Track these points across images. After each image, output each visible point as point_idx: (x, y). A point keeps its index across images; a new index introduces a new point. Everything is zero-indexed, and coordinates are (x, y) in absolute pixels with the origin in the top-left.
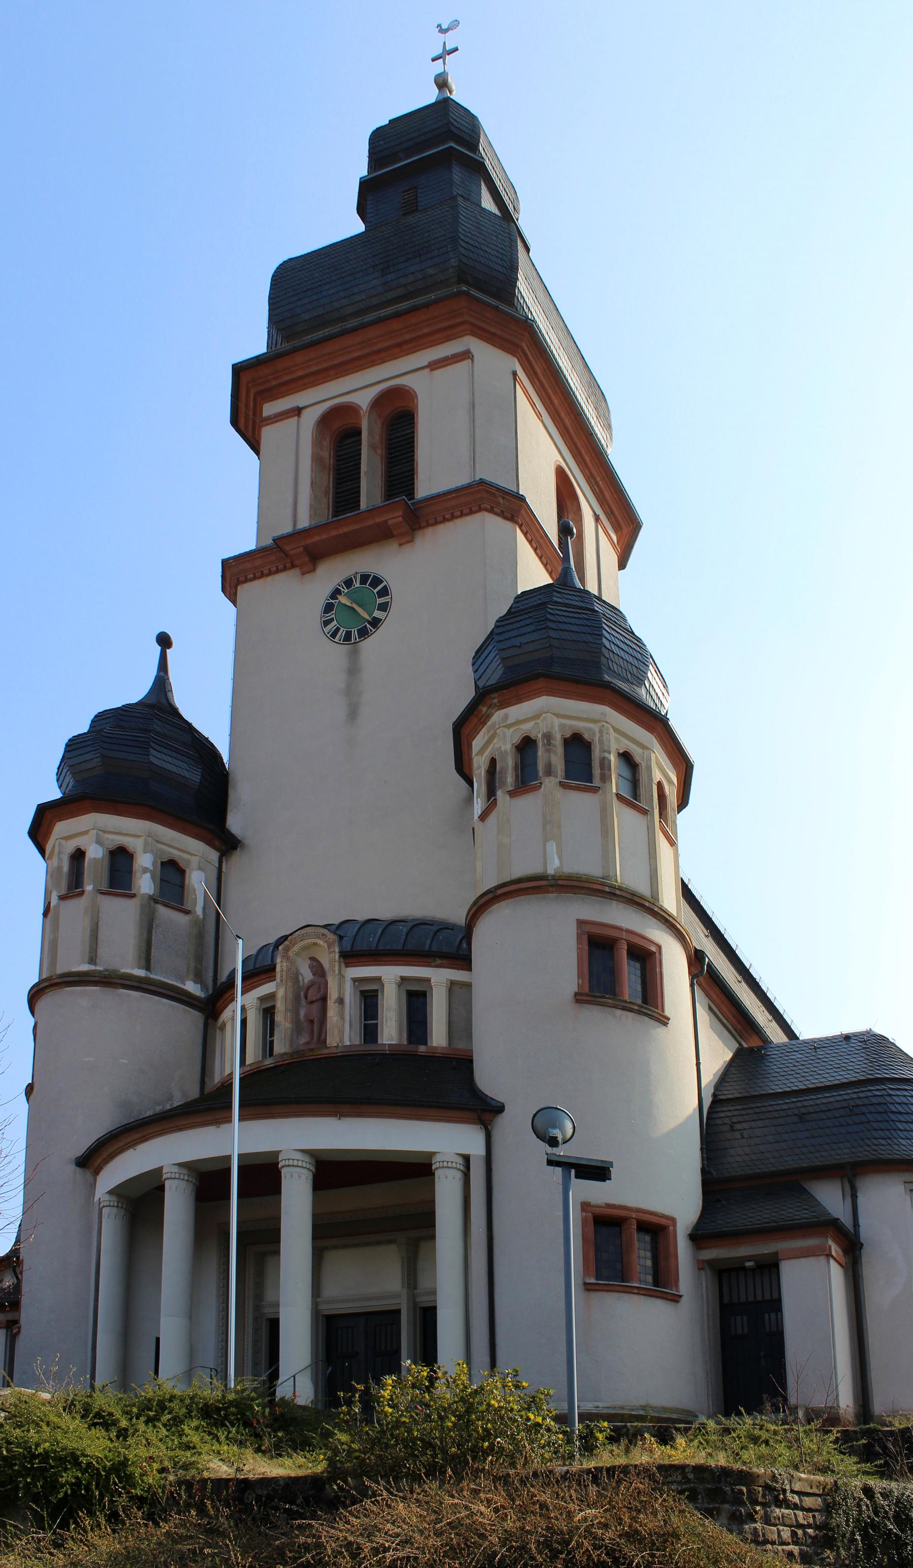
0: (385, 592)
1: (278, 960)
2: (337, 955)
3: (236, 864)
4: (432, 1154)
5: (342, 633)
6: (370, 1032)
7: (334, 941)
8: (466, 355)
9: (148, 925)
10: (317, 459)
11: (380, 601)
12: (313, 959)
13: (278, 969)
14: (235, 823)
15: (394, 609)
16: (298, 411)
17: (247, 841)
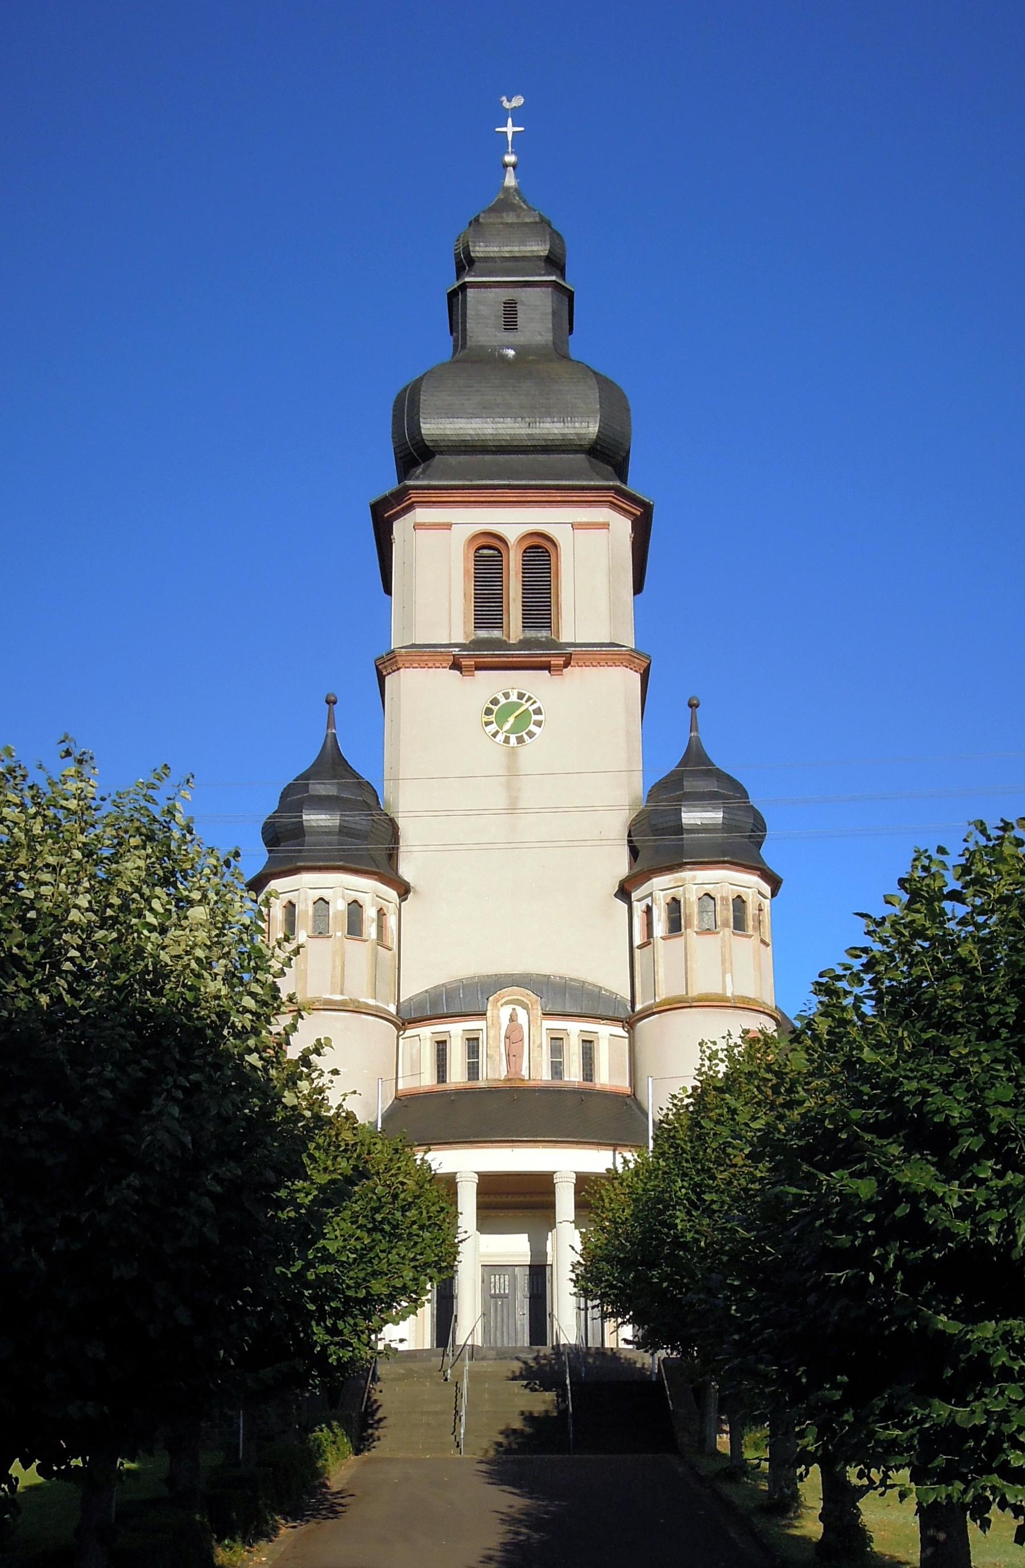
1: (489, 1008)
2: (540, 1013)
6: (557, 1070)
7: (537, 1001)
8: (605, 526)
9: (375, 956)
10: (466, 572)
12: (514, 1009)
13: (489, 1014)
16: (448, 526)
17: (417, 889)
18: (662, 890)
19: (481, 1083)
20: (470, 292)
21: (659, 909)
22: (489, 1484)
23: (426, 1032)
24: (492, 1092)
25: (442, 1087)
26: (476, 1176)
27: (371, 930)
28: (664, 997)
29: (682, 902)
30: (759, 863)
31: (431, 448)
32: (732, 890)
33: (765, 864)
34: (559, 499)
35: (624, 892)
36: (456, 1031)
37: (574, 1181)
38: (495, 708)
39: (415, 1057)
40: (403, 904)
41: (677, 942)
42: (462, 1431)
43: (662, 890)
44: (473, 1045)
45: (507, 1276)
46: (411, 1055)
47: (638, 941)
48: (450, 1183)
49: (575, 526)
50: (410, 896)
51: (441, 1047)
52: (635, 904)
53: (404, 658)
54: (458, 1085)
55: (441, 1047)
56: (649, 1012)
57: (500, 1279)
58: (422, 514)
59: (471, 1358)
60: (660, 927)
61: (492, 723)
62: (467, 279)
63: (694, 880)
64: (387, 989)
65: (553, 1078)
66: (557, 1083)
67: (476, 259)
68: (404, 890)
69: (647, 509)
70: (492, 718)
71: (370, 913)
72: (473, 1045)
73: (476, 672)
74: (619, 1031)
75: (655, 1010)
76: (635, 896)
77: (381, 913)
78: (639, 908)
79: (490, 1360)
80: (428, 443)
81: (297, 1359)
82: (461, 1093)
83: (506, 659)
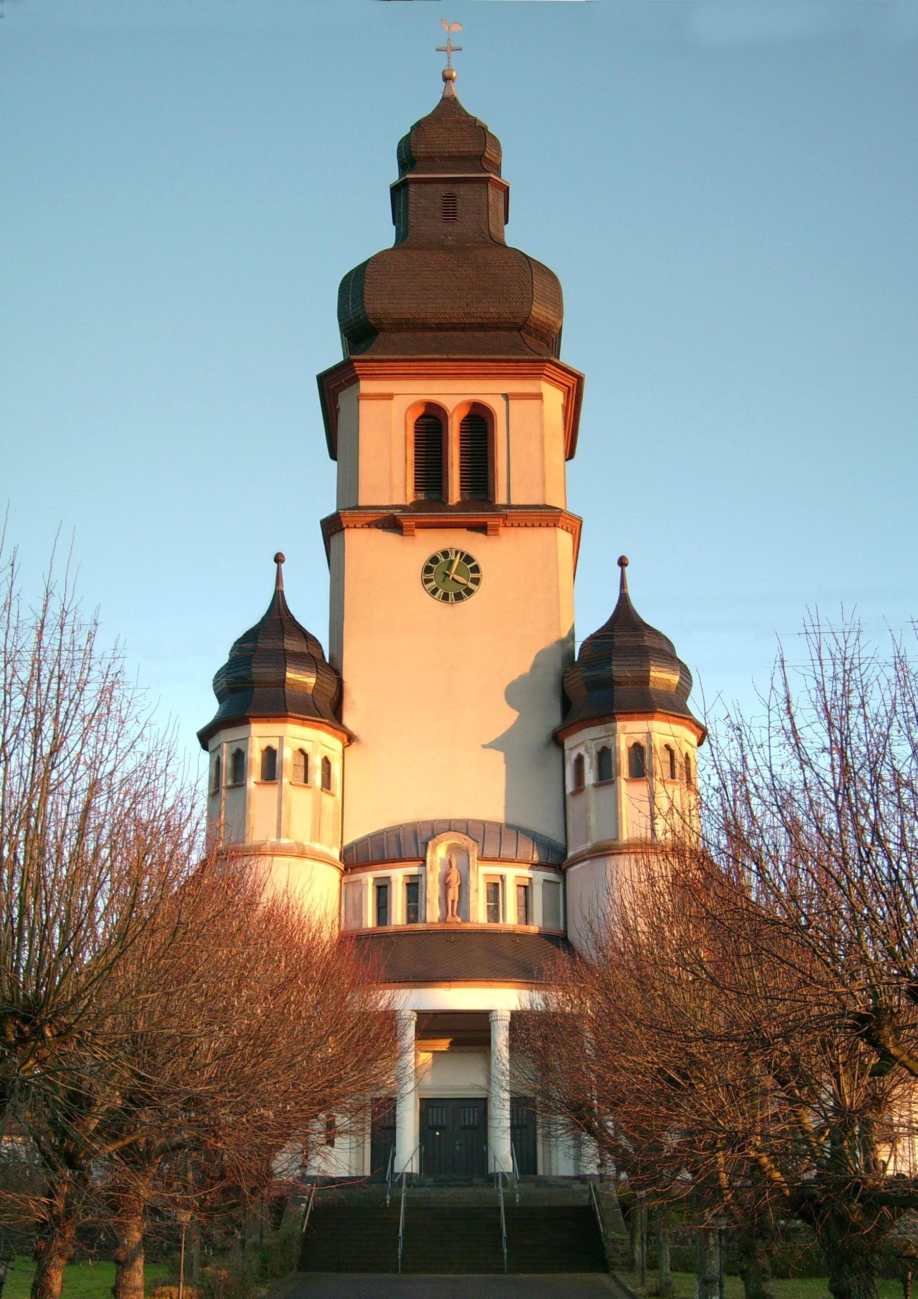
0: (476, 569)
3: (352, 750)
4: (491, 1011)
5: (440, 592)
11: (472, 575)
14: (350, 720)
15: (483, 583)
16: (389, 397)
17: (361, 738)
18: (593, 740)
19: (420, 926)
20: (412, 188)
21: (591, 757)
22: (118, 639)
23: (369, 878)
24: (429, 934)
25: (383, 929)
26: (415, 1014)
27: (317, 777)
28: (595, 841)
29: (613, 750)
30: (684, 713)
31: (375, 326)
32: (660, 739)
33: (692, 715)
34: (495, 372)
35: (557, 740)
36: (398, 875)
37: (509, 1019)
38: (435, 566)
39: (357, 901)
40: (346, 749)
41: (606, 792)
42: (400, 1252)
43: (593, 740)
44: (414, 887)
45: (476, 1109)
46: (353, 898)
47: (570, 788)
48: (390, 1018)
49: (506, 397)
50: (354, 744)
51: (383, 889)
52: (567, 752)
53: (348, 519)
54: (398, 928)
55: (383, 889)
56: (581, 858)
57: (437, 1112)
58: (366, 386)
59: (408, 1186)
60: (590, 777)
61: (431, 580)
62: (408, 176)
63: (624, 730)
64: (329, 832)
65: (489, 921)
66: (494, 926)
67: (417, 159)
68: (350, 739)
69: (580, 379)
70: (431, 576)
71: (316, 762)
72: (414, 887)
73: (416, 530)
74: (551, 876)
75: (586, 857)
76: (568, 743)
77: (326, 762)
78: (571, 757)
79: (428, 1187)
80: (372, 321)
81: (273, 1165)
82: (399, 934)
83: (445, 520)
